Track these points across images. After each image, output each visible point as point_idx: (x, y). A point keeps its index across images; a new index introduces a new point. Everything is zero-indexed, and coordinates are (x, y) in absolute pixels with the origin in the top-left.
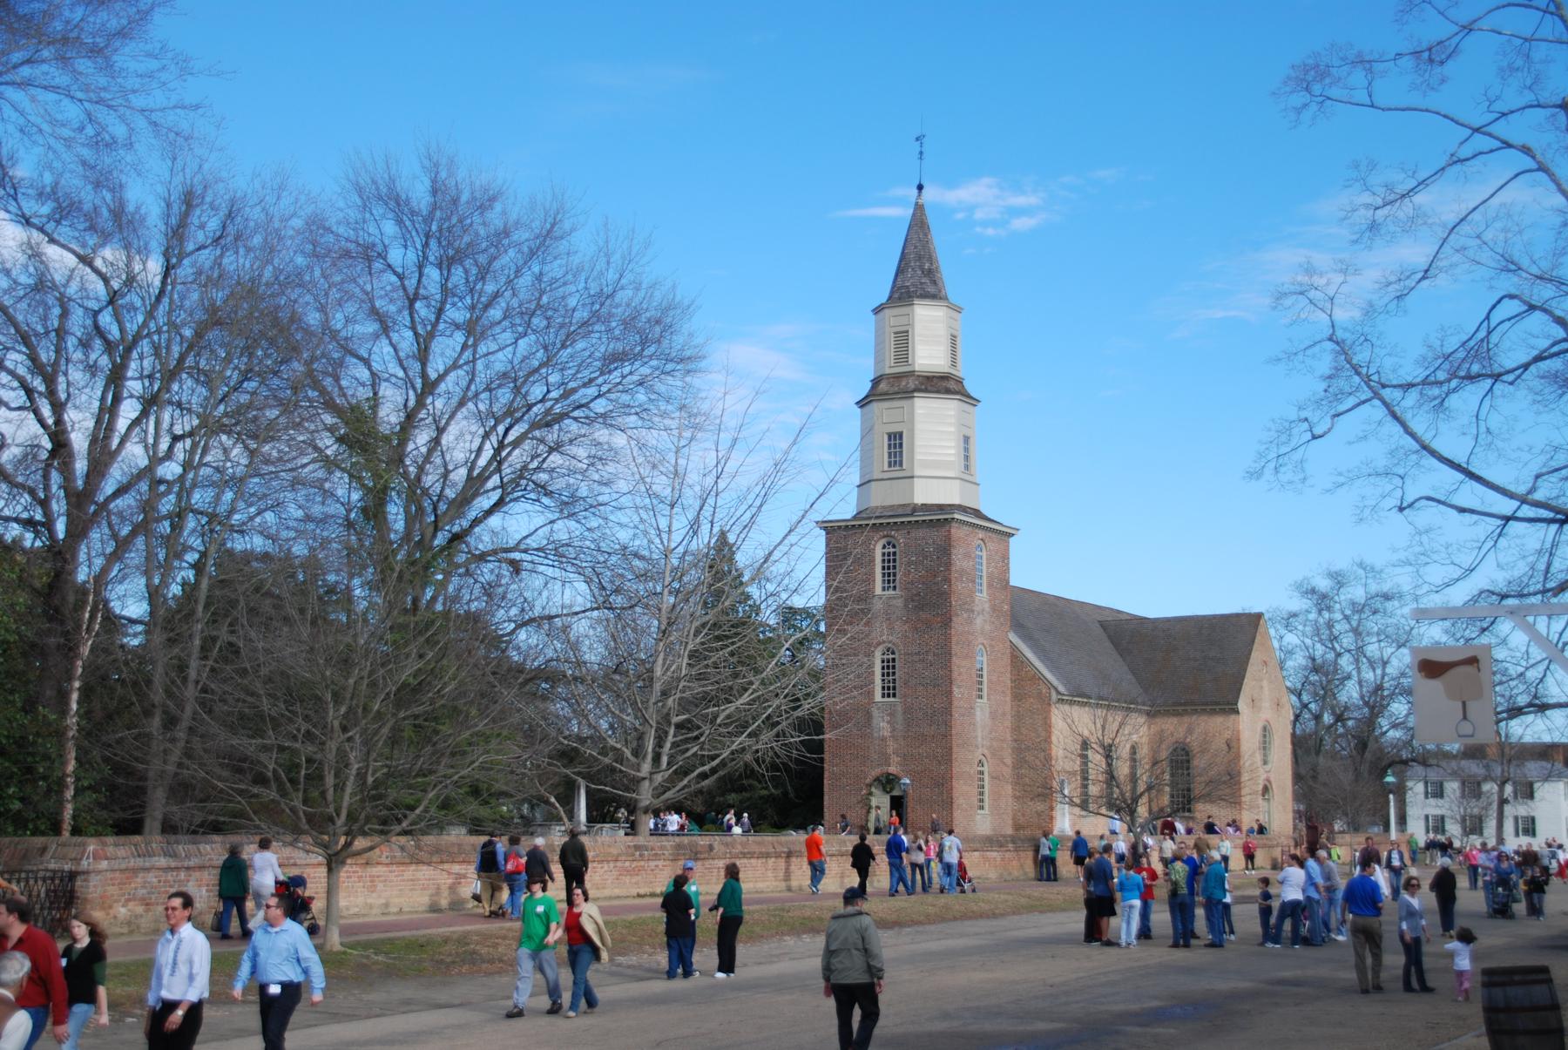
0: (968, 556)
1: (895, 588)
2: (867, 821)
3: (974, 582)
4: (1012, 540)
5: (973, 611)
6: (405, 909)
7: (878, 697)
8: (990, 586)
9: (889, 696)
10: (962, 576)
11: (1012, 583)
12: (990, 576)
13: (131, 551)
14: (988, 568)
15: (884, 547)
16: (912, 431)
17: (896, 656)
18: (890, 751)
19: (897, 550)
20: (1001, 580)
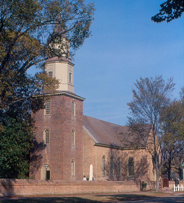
0: (69, 104)
1: (49, 113)
2: (120, 181)
3: (71, 112)
4: (83, 101)
5: (71, 120)
6: (95, 192)
7: (45, 114)
8: (76, 113)
9: (48, 113)
10: (67, 110)
11: (84, 114)
12: (76, 111)
13: (42, 163)
14: (76, 108)
15: (46, 131)
16: (55, 71)
17: (49, 132)
18: (47, 158)
19: (49, 132)
20: (80, 113)
